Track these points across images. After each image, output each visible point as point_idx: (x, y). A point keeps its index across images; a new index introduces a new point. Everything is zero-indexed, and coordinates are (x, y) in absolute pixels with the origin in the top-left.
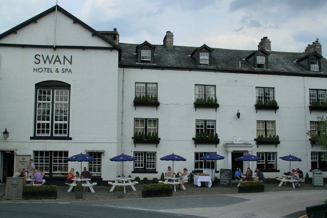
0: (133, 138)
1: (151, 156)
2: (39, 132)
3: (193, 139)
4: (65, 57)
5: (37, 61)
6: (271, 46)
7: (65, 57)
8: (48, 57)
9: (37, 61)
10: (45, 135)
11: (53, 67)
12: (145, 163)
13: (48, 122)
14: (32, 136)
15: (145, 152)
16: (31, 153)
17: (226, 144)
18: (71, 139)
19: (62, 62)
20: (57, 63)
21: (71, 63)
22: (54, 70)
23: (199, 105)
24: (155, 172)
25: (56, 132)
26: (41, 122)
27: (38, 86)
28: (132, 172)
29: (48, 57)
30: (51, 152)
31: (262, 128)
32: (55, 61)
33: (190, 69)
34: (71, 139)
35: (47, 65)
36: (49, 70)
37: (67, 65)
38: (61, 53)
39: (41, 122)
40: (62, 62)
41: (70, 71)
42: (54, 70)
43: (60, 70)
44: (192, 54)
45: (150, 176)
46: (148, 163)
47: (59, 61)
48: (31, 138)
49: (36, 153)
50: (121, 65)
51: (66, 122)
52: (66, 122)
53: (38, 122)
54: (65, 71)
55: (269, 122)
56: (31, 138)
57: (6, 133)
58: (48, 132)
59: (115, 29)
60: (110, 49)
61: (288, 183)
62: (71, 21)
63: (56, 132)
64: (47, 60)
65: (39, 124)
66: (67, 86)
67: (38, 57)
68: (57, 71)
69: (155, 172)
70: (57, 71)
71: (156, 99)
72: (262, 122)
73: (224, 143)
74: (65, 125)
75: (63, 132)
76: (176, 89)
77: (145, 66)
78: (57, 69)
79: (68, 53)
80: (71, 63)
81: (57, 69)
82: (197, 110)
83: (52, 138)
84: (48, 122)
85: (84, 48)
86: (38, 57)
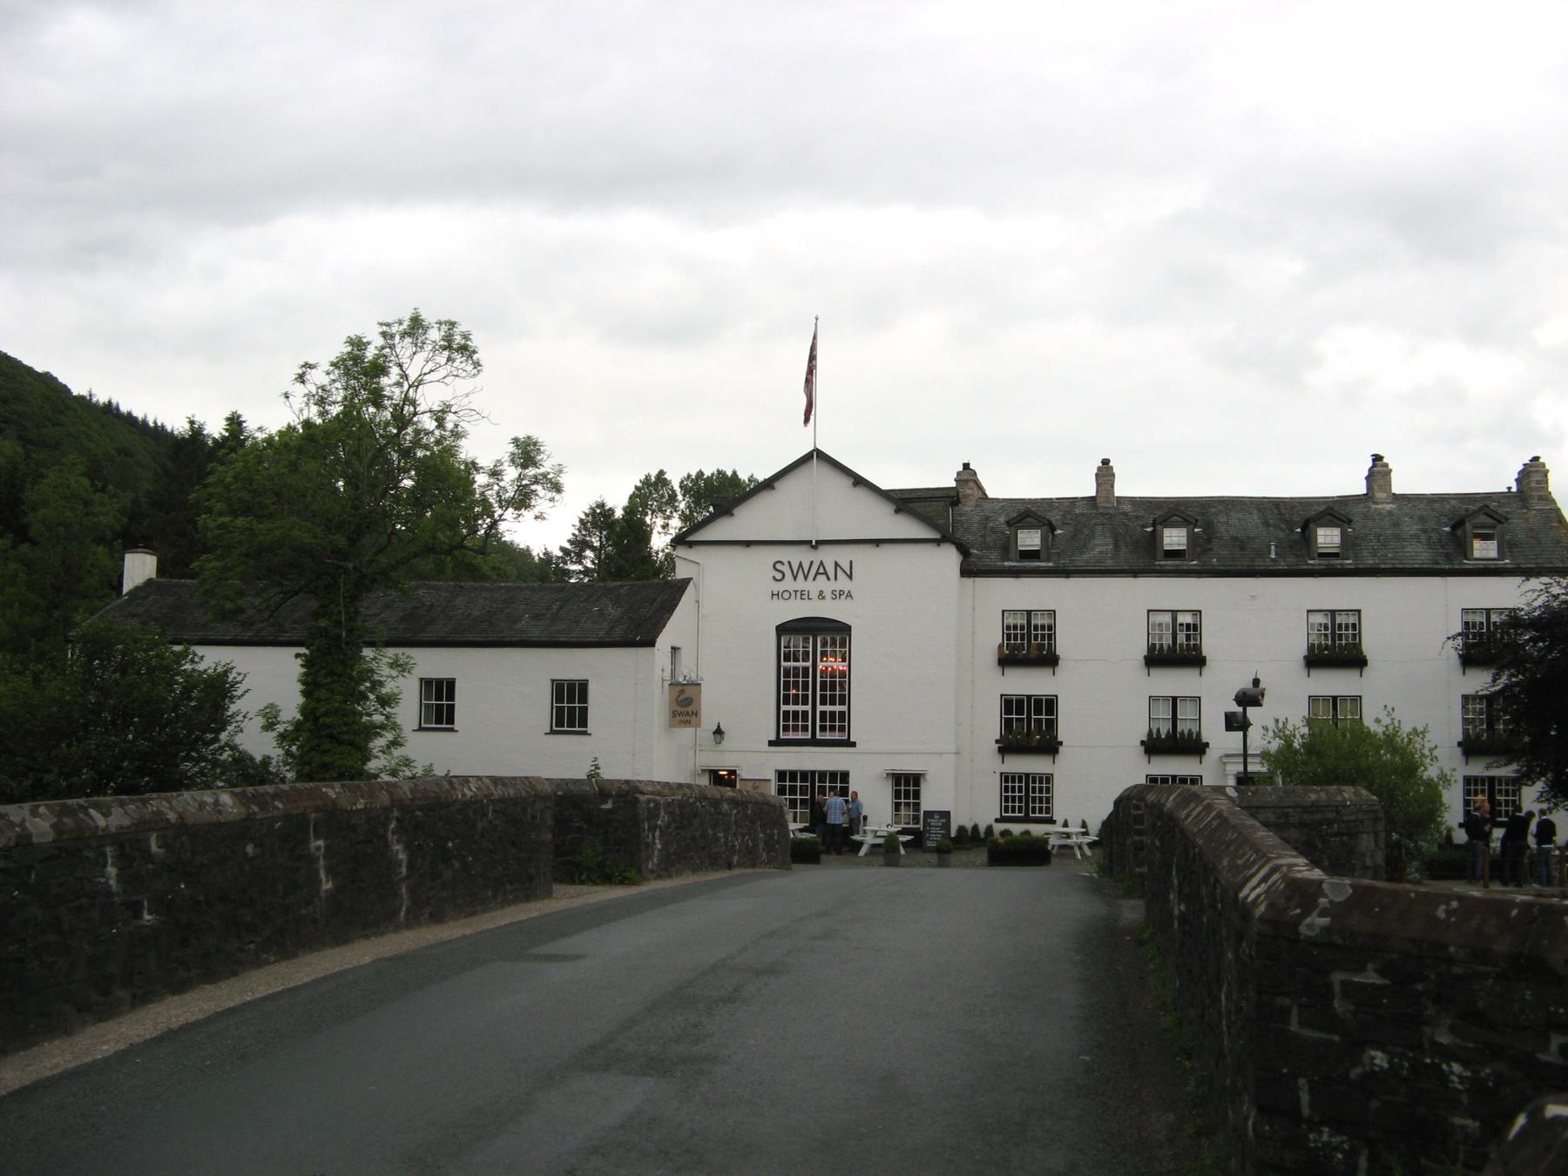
0: (1460, 744)
1: (907, 784)
2: (786, 728)
3: (1143, 743)
4: (837, 565)
5: (779, 576)
6: (1554, 495)
7: (837, 565)
8: (801, 565)
9: (779, 576)
10: (800, 736)
11: (813, 587)
12: (1028, 796)
13: (824, 708)
14: (773, 738)
15: (1027, 775)
16: (772, 776)
17: (1227, 756)
18: (853, 745)
19: (832, 575)
20: (822, 578)
21: (850, 577)
22: (814, 595)
23: (1157, 659)
24: (1051, 821)
25: (823, 729)
26: (791, 708)
27: (782, 630)
28: (997, 821)
29: (801, 565)
30: (813, 773)
31: (1164, 712)
32: (817, 573)
33: (1135, 573)
34: (853, 745)
35: (800, 584)
36: (803, 595)
37: (843, 583)
38: (828, 556)
39: (791, 708)
40: (832, 575)
41: (849, 595)
42: (814, 595)
43: (828, 594)
44: (1454, 528)
45: (1037, 830)
46: (1034, 799)
47: (825, 573)
48: (771, 743)
49: (781, 775)
50: (967, 571)
51: (844, 708)
52: (844, 708)
53: (784, 708)
54: (838, 595)
55: (1344, 698)
56: (771, 743)
57: (719, 732)
58: (805, 729)
59: (1533, 473)
60: (938, 542)
61: (1061, 847)
62: (850, 482)
63: (823, 729)
64: (799, 571)
65: (786, 713)
66: (845, 629)
67: (779, 566)
68: (821, 596)
69: (1051, 821)
70: (821, 596)
71: (1357, 647)
72: (1325, 699)
73: (1222, 752)
74: (842, 714)
75: (836, 729)
76: (1103, 619)
77: (1331, 567)
78: (821, 593)
79: (843, 555)
80: (850, 577)
81: (821, 593)
82: (1313, 672)
83: (814, 742)
84: (824, 708)
85: (877, 542)
86: (779, 566)
